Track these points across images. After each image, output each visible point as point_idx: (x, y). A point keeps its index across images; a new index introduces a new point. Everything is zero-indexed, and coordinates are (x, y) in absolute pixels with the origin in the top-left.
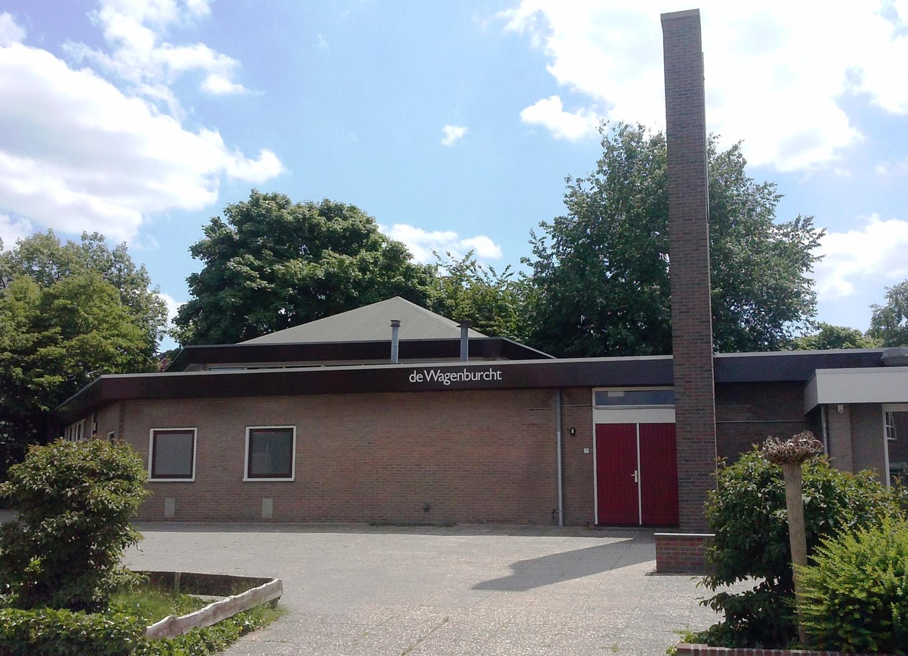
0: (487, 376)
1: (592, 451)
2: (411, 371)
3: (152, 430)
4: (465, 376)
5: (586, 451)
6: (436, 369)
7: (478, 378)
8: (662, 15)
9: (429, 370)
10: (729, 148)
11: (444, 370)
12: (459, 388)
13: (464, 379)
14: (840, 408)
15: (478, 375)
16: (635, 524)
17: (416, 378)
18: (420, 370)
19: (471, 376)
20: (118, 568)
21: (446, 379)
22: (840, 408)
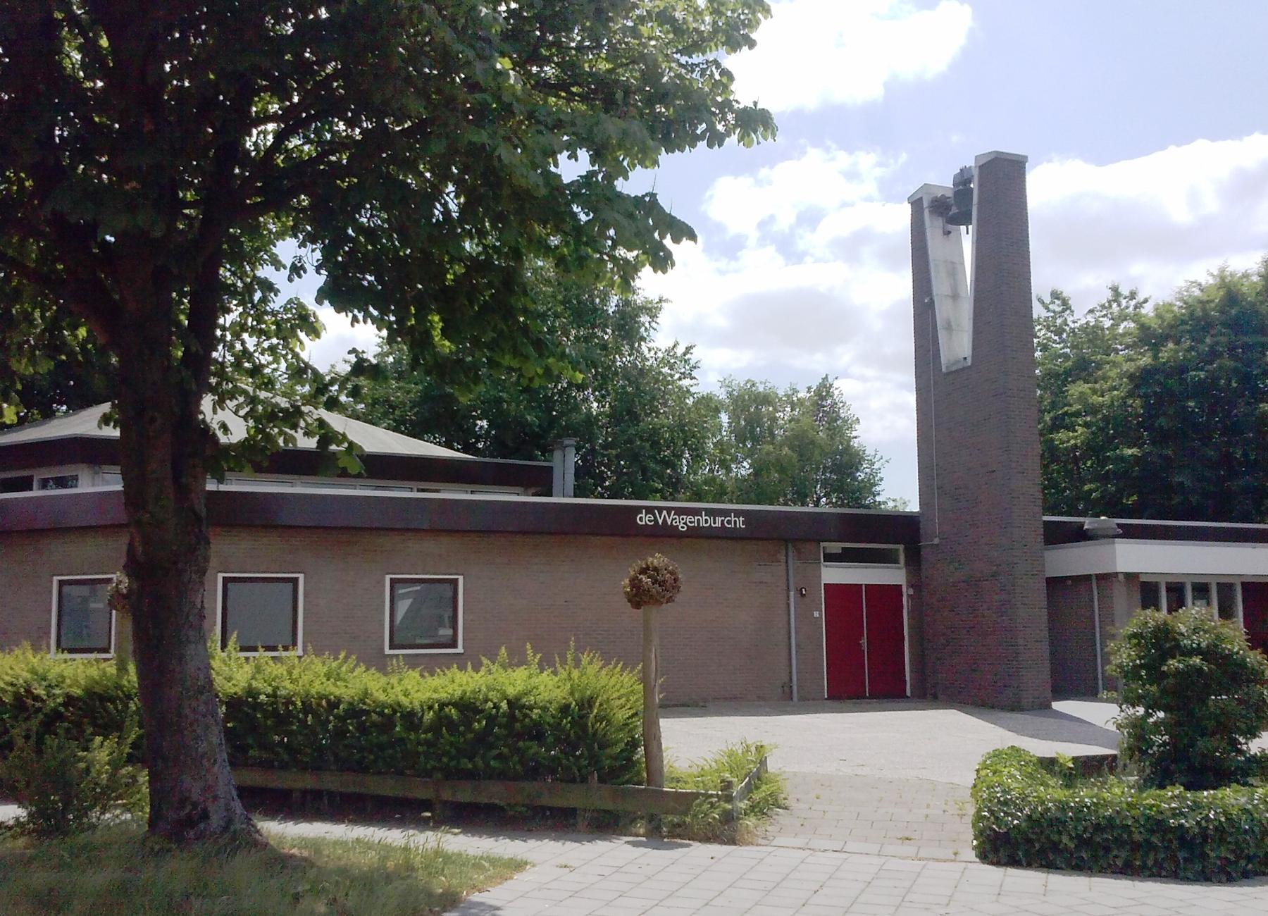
0: (729, 522)
1: (820, 614)
2: (638, 510)
3: (56, 579)
4: (704, 521)
5: (816, 614)
6: (669, 510)
7: (718, 524)
8: (1026, 157)
9: (660, 509)
10: (671, 345)
11: (680, 512)
12: (695, 533)
13: (702, 524)
14: (1121, 577)
15: (719, 520)
16: (864, 697)
17: (644, 519)
18: (650, 510)
19: (711, 520)
20: (621, 716)
21: (682, 523)
22: (1121, 577)
